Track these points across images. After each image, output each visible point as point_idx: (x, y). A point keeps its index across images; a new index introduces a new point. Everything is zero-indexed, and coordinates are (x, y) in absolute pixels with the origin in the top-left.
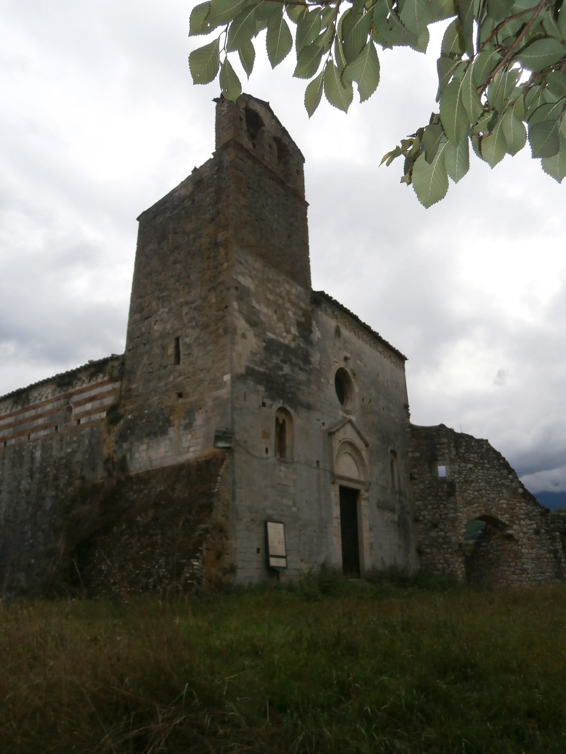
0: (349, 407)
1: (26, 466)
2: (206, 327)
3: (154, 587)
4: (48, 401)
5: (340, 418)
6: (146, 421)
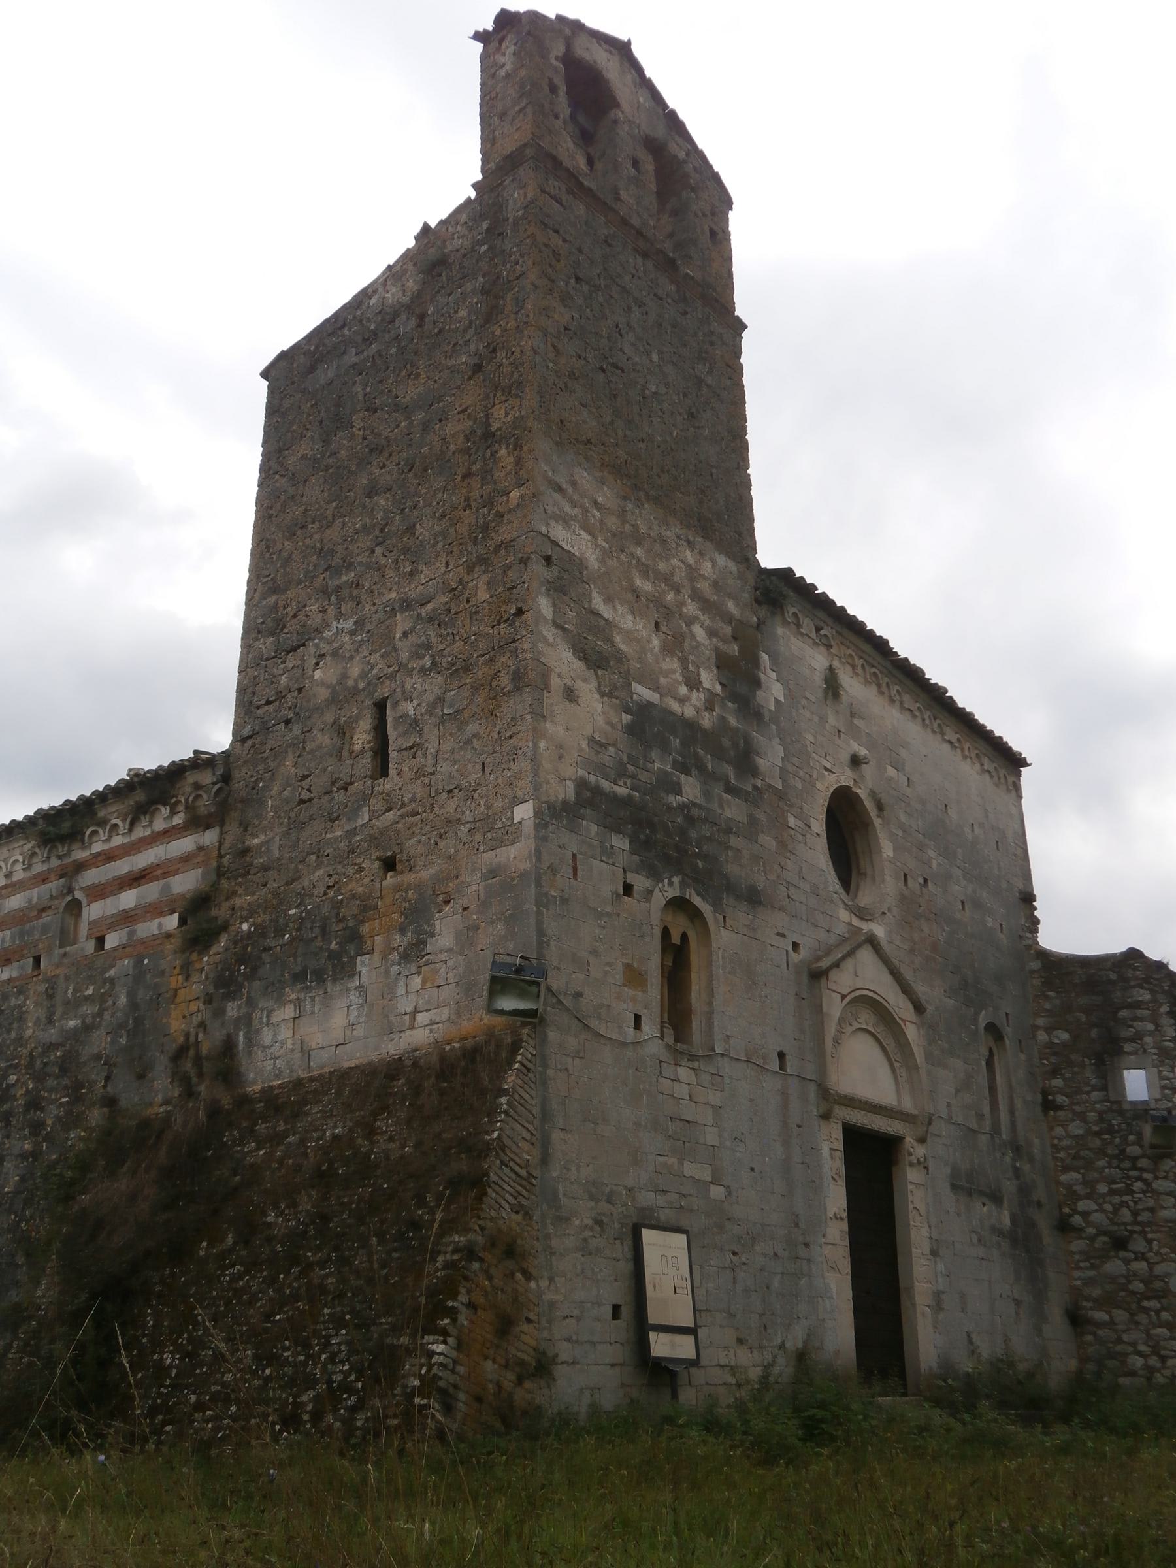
0: (865, 898)
3: (317, 1416)
5: (841, 929)
6: (293, 939)
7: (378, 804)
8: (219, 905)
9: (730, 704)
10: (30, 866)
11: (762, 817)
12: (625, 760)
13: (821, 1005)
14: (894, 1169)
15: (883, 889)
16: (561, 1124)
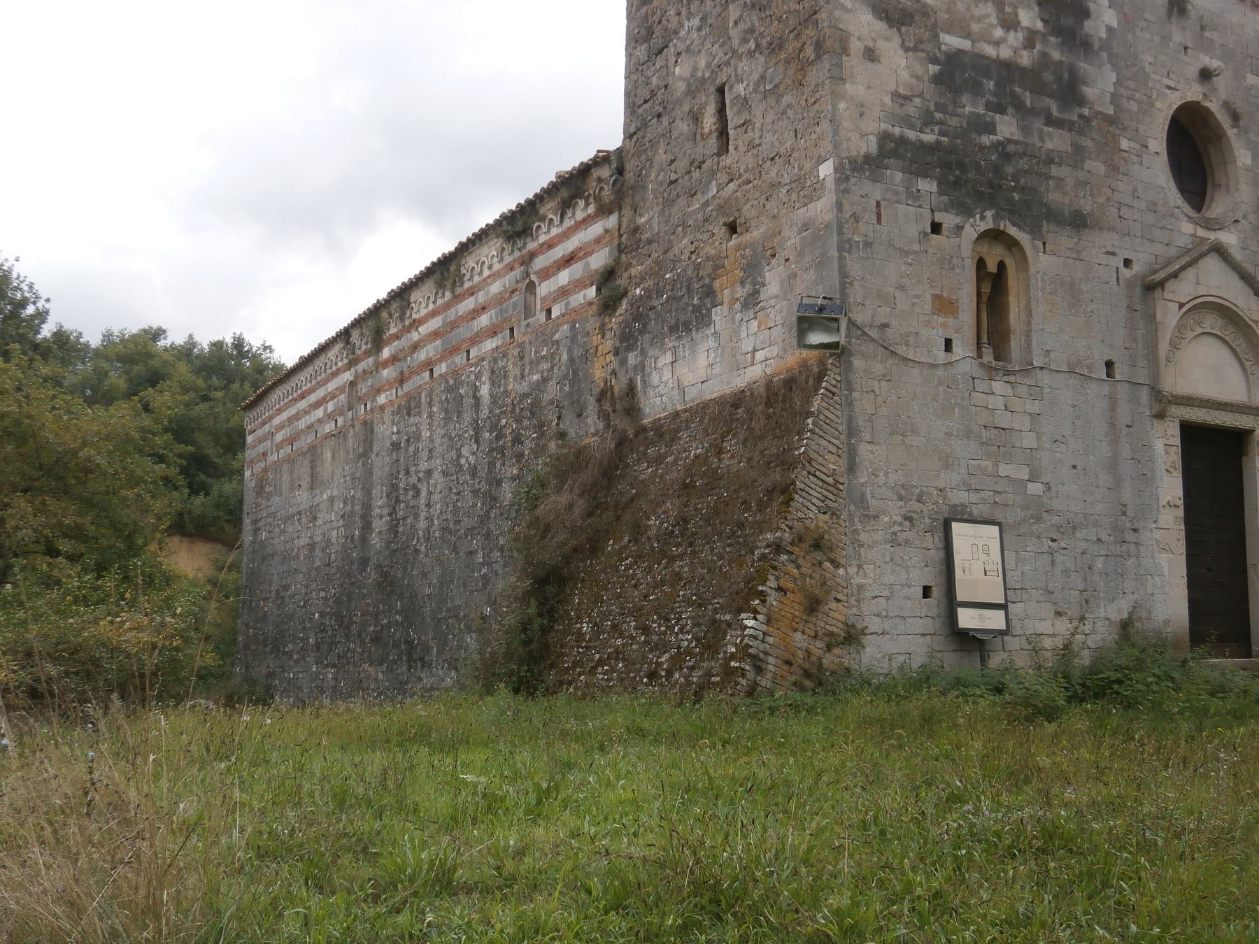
0: (1218, 207)
1: (467, 418)
2: (776, 47)
3: (670, 673)
4: (492, 271)
5: (1183, 242)
6: (668, 298)
7: (722, 178)
8: (620, 276)
9: (1053, 39)
10: (502, 259)
11: (1088, 143)
12: (932, 108)
13: (1155, 315)
14: (1244, 458)
15: (1237, 196)
16: (867, 437)
